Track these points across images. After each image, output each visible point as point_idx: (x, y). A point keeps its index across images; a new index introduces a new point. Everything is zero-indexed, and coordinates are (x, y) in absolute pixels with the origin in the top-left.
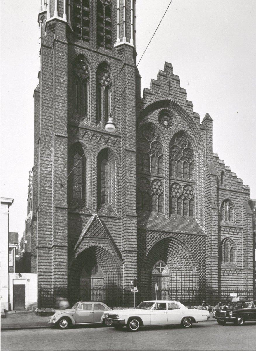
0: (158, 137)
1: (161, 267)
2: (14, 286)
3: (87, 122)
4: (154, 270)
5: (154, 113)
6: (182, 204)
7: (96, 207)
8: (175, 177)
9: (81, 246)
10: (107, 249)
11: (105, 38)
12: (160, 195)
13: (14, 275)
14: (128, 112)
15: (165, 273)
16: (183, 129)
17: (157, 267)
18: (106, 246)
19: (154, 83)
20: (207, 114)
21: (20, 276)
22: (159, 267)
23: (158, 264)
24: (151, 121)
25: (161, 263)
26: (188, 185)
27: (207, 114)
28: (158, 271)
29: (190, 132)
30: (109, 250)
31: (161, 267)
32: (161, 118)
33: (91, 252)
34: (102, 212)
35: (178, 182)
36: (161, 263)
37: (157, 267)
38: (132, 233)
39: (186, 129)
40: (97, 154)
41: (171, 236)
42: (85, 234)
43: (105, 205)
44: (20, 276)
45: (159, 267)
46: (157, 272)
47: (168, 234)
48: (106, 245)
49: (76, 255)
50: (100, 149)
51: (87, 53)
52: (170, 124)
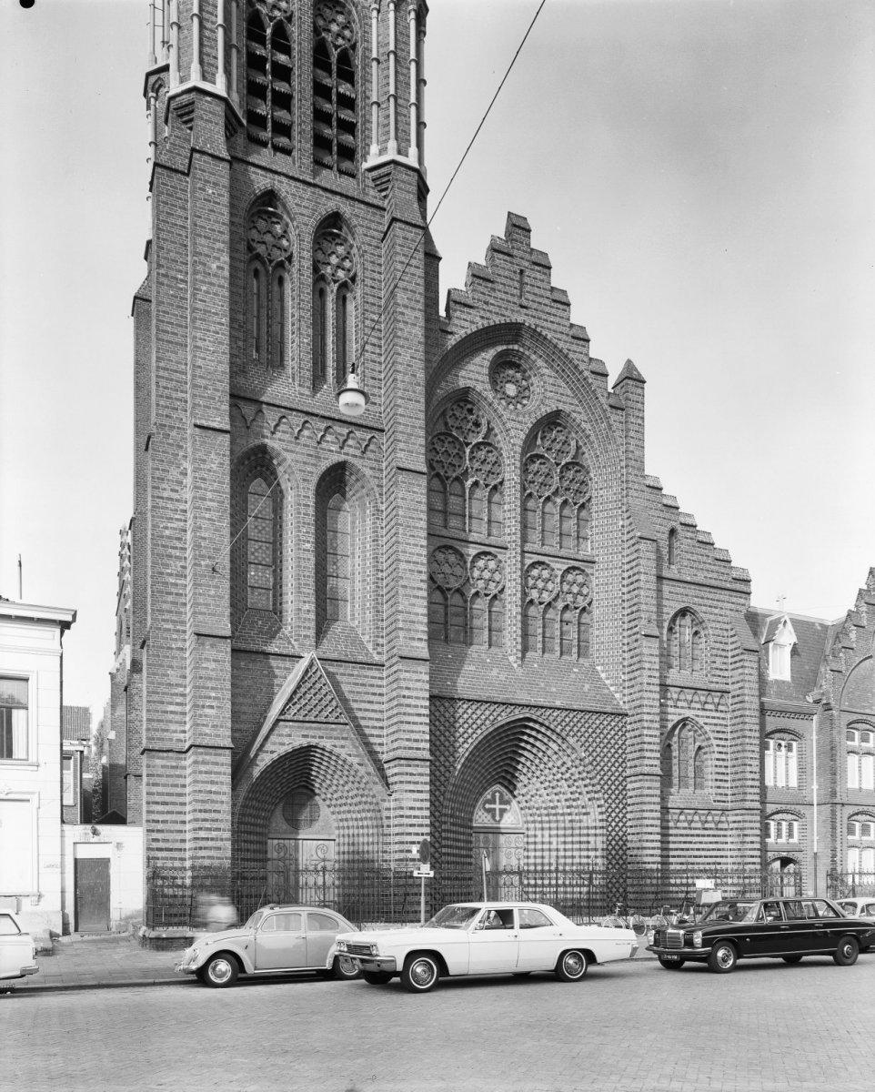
0: (490, 430)
1: (497, 806)
2: (76, 860)
3: (286, 388)
4: (480, 813)
5: (477, 360)
6: (558, 617)
7: (312, 633)
8: (537, 547)
9: (268, 747)
10: (343, 753)
11: (336, 144)
12: (495, 597)
13: (79, 831)
14: (405, 357)
15: (509, 821)
16: (561, 406)
17: (487, 806)
18: (343, 747)
19: (478, 276)
20: (629, 362)
21: (95, 833)
22: (492, 806)
23: (489, 797)
24: (470, 384)
25: (497, 794)
26: (574, 568)
27: (629, 362)
28: (489, 817)
29: (580, 416)
30: (350, 755)
31: (497, 806)
32: (503, 364)
33: (301, 760)
34: (330, 648)
35: (492, 550)
36: (497, 794)
37: (487, 806)
38: (416, 706)
39: (567, 408)
40: (315, 479)
41: (528, 715)
42: (282, 712)
43: (337, 628)
44: (95, 833)
45: (492, 806)
46: (486, 821)
47: (517, 711)
48: (343, 742)
49: (256, 772)
50: (325, 465)
51: (284, 188)
52: (523, 394)
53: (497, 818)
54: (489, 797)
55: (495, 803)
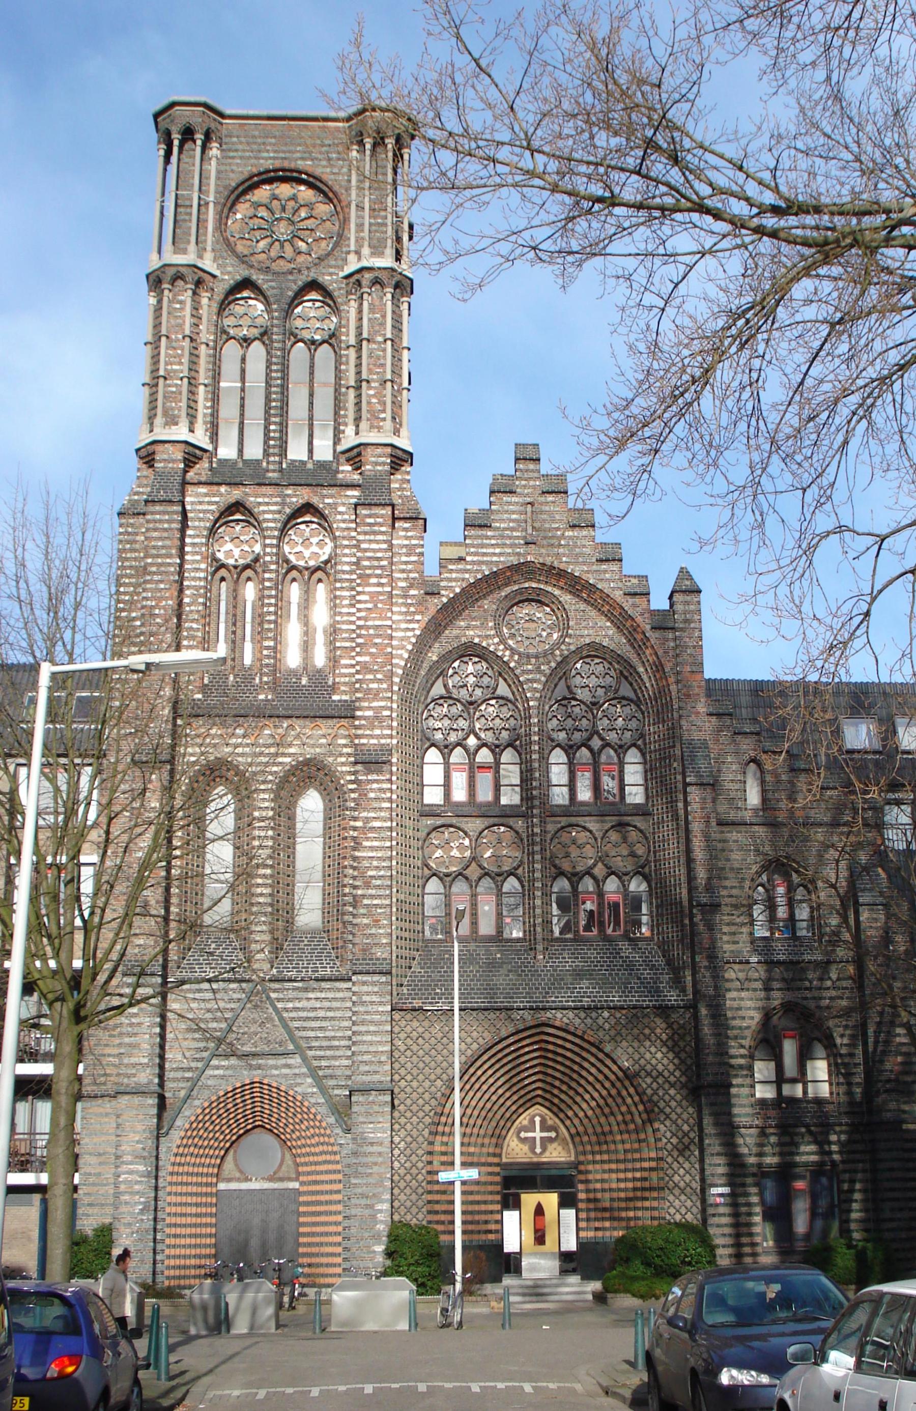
23: (525, 1122)
25: (537, 1119)
28: (526, 1148)
36: (537, 1119)
37: (523, 1135)
53: (538, 1150)
54: (525, 1122)
55: (542, 1130)
